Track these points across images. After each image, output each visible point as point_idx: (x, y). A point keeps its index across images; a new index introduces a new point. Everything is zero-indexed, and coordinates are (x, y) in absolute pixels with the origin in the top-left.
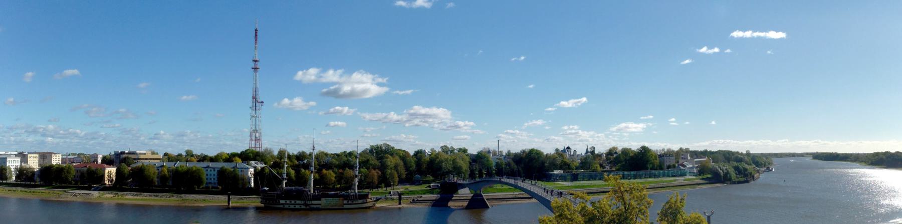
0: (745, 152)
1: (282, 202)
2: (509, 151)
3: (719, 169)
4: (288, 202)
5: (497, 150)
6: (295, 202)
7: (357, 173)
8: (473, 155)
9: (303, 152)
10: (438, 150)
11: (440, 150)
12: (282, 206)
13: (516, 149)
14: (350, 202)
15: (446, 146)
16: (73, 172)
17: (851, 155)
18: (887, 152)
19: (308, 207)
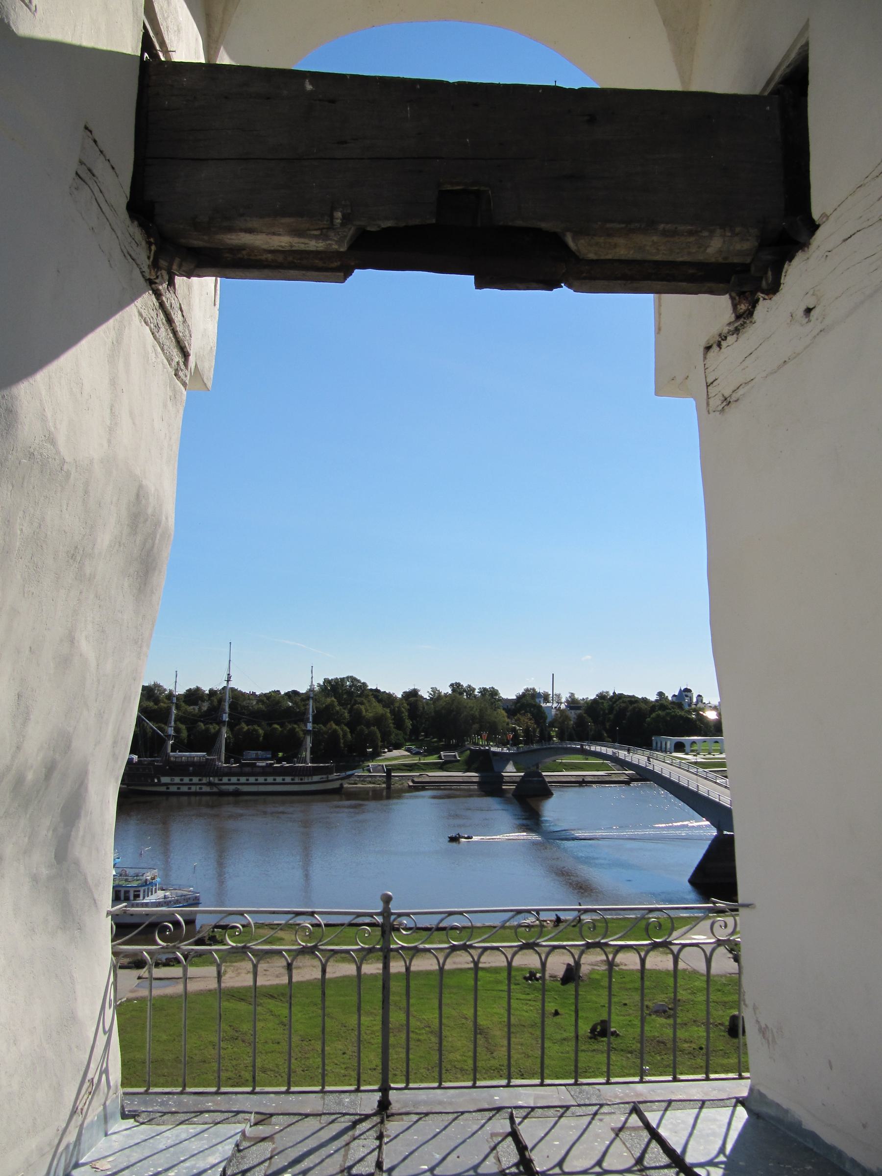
0: (653, 697)
1: (165, 780)
2: (572, 694)
3: (622, 754)
4: (177, 780)
5: (550, 692)
6: (191, 780)
7: (171, 731)
8: (507, 700)
9: (198, 689)
10: (446, 690)
11: (449, 691)
12: (163, 789)
13: (587, 693)
14: (297, 780)
15: (459, 684)
16: (554, 712)
17: (784, 56)
18: (618, 698)
19: (215, 790)
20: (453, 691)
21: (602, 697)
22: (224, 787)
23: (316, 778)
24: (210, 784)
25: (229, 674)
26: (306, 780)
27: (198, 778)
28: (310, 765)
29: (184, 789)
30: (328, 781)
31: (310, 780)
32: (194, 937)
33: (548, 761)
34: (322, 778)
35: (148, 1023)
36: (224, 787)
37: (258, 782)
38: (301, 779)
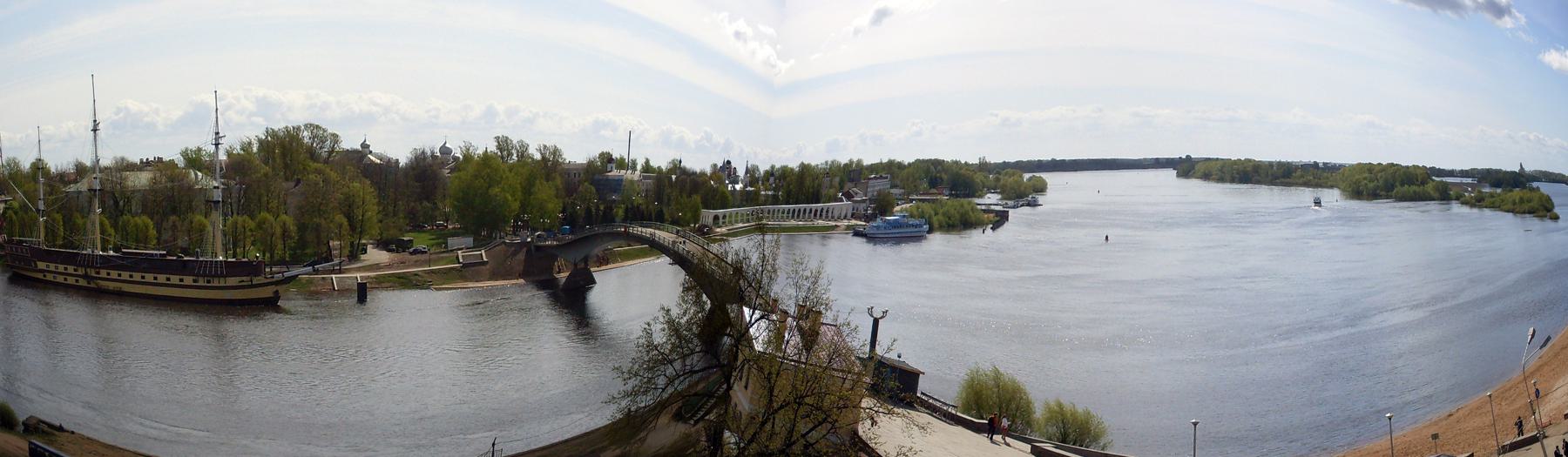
1: (41, 265)
20: (499, 147)
21: (918, 161)
22: (103, 283)
23: (233, 281)
24: (85, 276)
25: (95, 121)
26: (215, 283)
27: (191, 278)
28: (111, 253)
29: (60, 279)
30: (252, 286)
31: (222, 284)
32: (1442, 181)
33: (597, 250)
34: (243, 281)
35: (480, 435)
36: (103, 283)
37: (121, 278)
38: (209, 282)
